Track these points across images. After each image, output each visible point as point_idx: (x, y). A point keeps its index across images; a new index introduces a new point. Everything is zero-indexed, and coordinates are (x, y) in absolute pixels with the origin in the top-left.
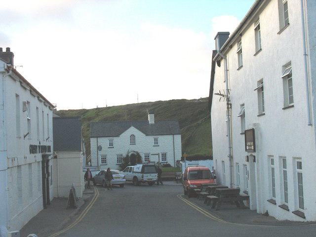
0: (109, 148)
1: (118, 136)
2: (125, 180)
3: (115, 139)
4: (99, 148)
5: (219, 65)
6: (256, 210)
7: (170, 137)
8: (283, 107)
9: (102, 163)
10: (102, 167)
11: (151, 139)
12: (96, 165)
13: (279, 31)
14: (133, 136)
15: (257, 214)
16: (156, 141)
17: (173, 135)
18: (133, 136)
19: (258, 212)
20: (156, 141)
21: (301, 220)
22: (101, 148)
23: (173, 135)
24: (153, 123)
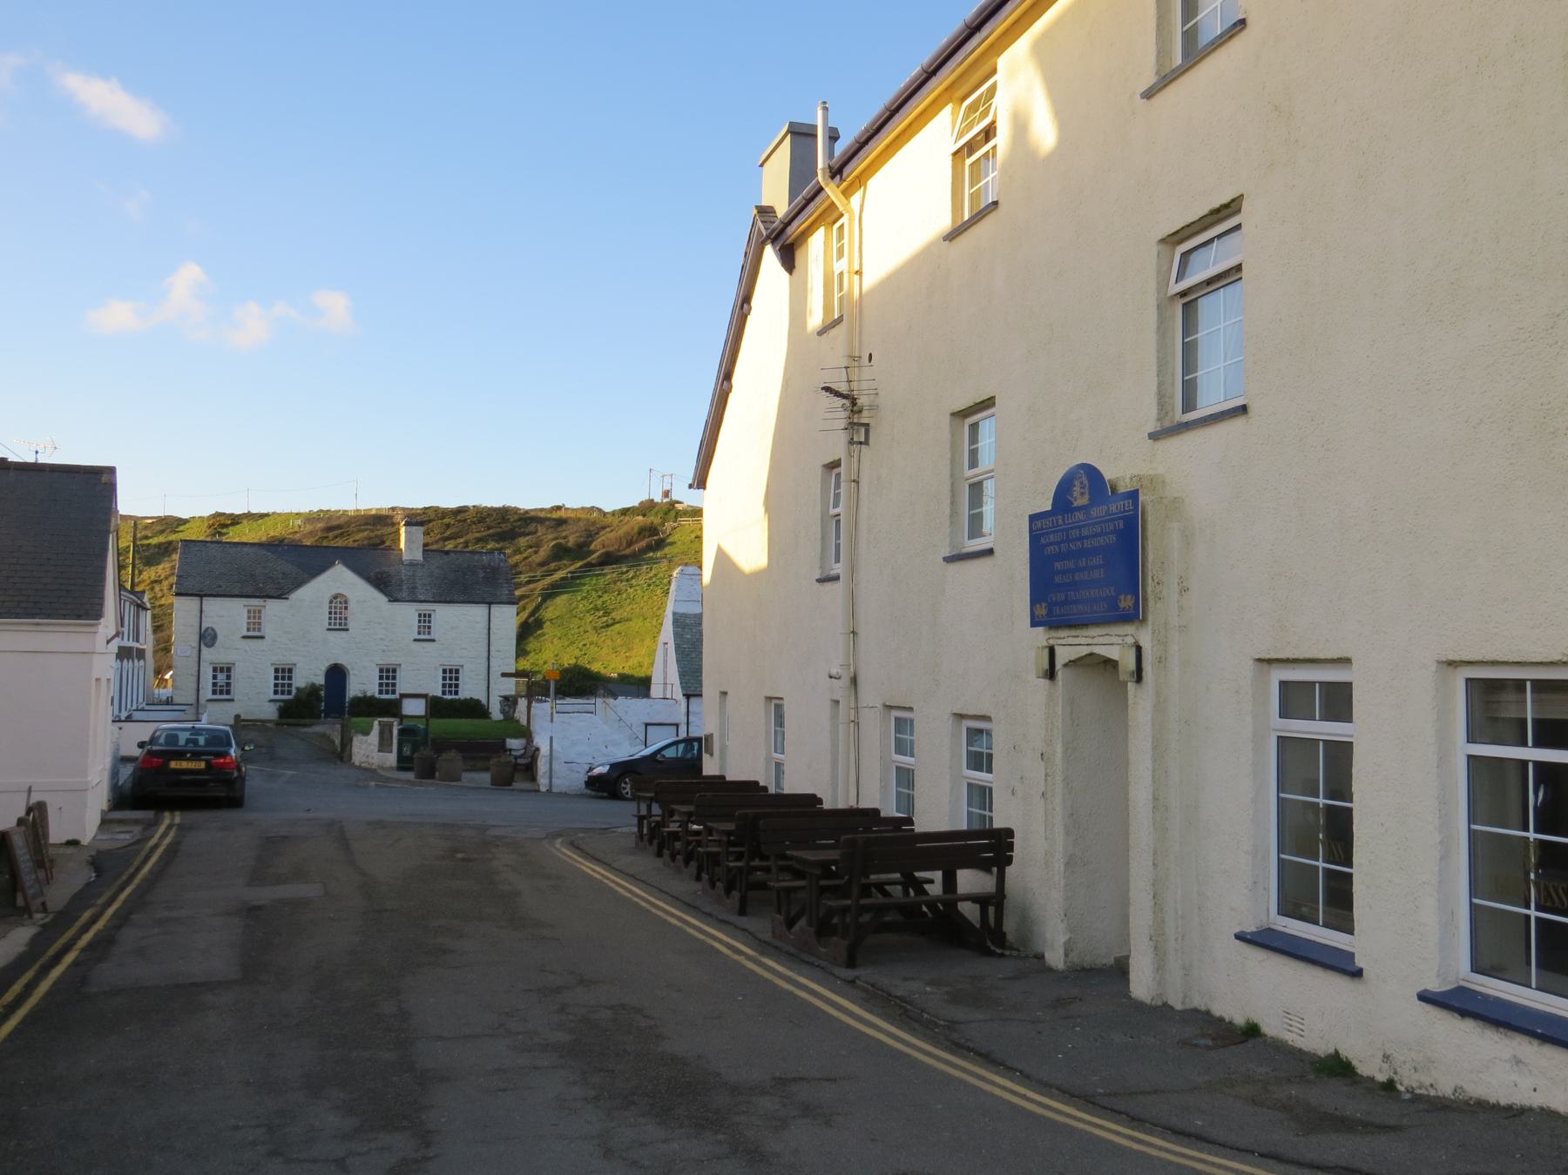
0: (245, 637)
1: (282, 593)
2: (202, 765)
3: (272, 608)
4: (207, 638)
5: (789, 258)
6: (1120, 970)
7: (477, 612)
8: (1152, 426)
9: (214, 692)
10: (212, 707)
11: (408, 613)
12: (192, 700)
13: (1149, 79)
14: (339, 604)
15: (1139, 1006)
16: (425, 620)
17: (490, 604)
18: (339, 604)
19: (1142, 985)
20: (425, 620)
21: (886, 900)
22: (214, 637)
23: (490, 604)
24: (418, 556)
